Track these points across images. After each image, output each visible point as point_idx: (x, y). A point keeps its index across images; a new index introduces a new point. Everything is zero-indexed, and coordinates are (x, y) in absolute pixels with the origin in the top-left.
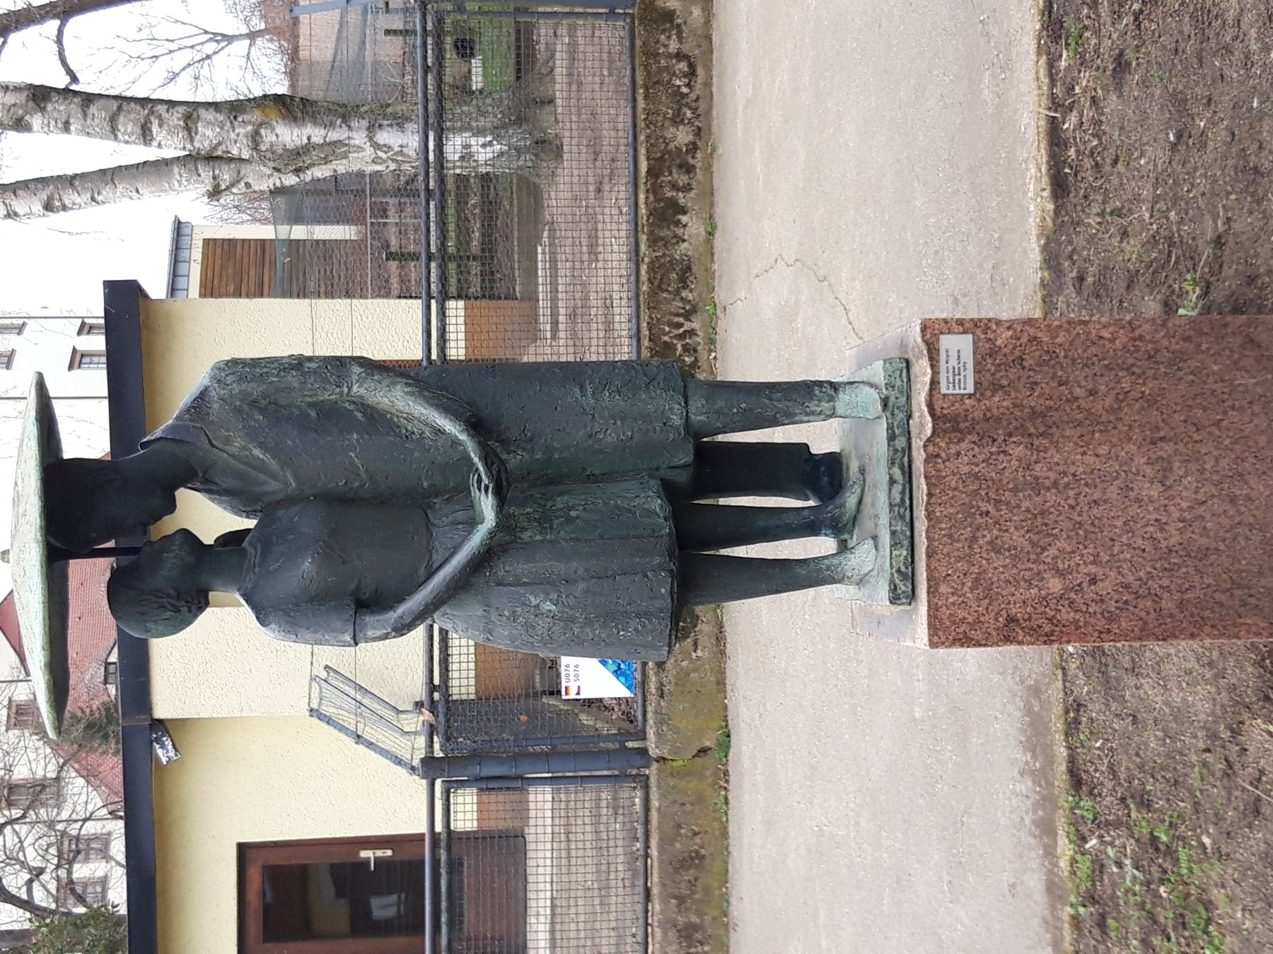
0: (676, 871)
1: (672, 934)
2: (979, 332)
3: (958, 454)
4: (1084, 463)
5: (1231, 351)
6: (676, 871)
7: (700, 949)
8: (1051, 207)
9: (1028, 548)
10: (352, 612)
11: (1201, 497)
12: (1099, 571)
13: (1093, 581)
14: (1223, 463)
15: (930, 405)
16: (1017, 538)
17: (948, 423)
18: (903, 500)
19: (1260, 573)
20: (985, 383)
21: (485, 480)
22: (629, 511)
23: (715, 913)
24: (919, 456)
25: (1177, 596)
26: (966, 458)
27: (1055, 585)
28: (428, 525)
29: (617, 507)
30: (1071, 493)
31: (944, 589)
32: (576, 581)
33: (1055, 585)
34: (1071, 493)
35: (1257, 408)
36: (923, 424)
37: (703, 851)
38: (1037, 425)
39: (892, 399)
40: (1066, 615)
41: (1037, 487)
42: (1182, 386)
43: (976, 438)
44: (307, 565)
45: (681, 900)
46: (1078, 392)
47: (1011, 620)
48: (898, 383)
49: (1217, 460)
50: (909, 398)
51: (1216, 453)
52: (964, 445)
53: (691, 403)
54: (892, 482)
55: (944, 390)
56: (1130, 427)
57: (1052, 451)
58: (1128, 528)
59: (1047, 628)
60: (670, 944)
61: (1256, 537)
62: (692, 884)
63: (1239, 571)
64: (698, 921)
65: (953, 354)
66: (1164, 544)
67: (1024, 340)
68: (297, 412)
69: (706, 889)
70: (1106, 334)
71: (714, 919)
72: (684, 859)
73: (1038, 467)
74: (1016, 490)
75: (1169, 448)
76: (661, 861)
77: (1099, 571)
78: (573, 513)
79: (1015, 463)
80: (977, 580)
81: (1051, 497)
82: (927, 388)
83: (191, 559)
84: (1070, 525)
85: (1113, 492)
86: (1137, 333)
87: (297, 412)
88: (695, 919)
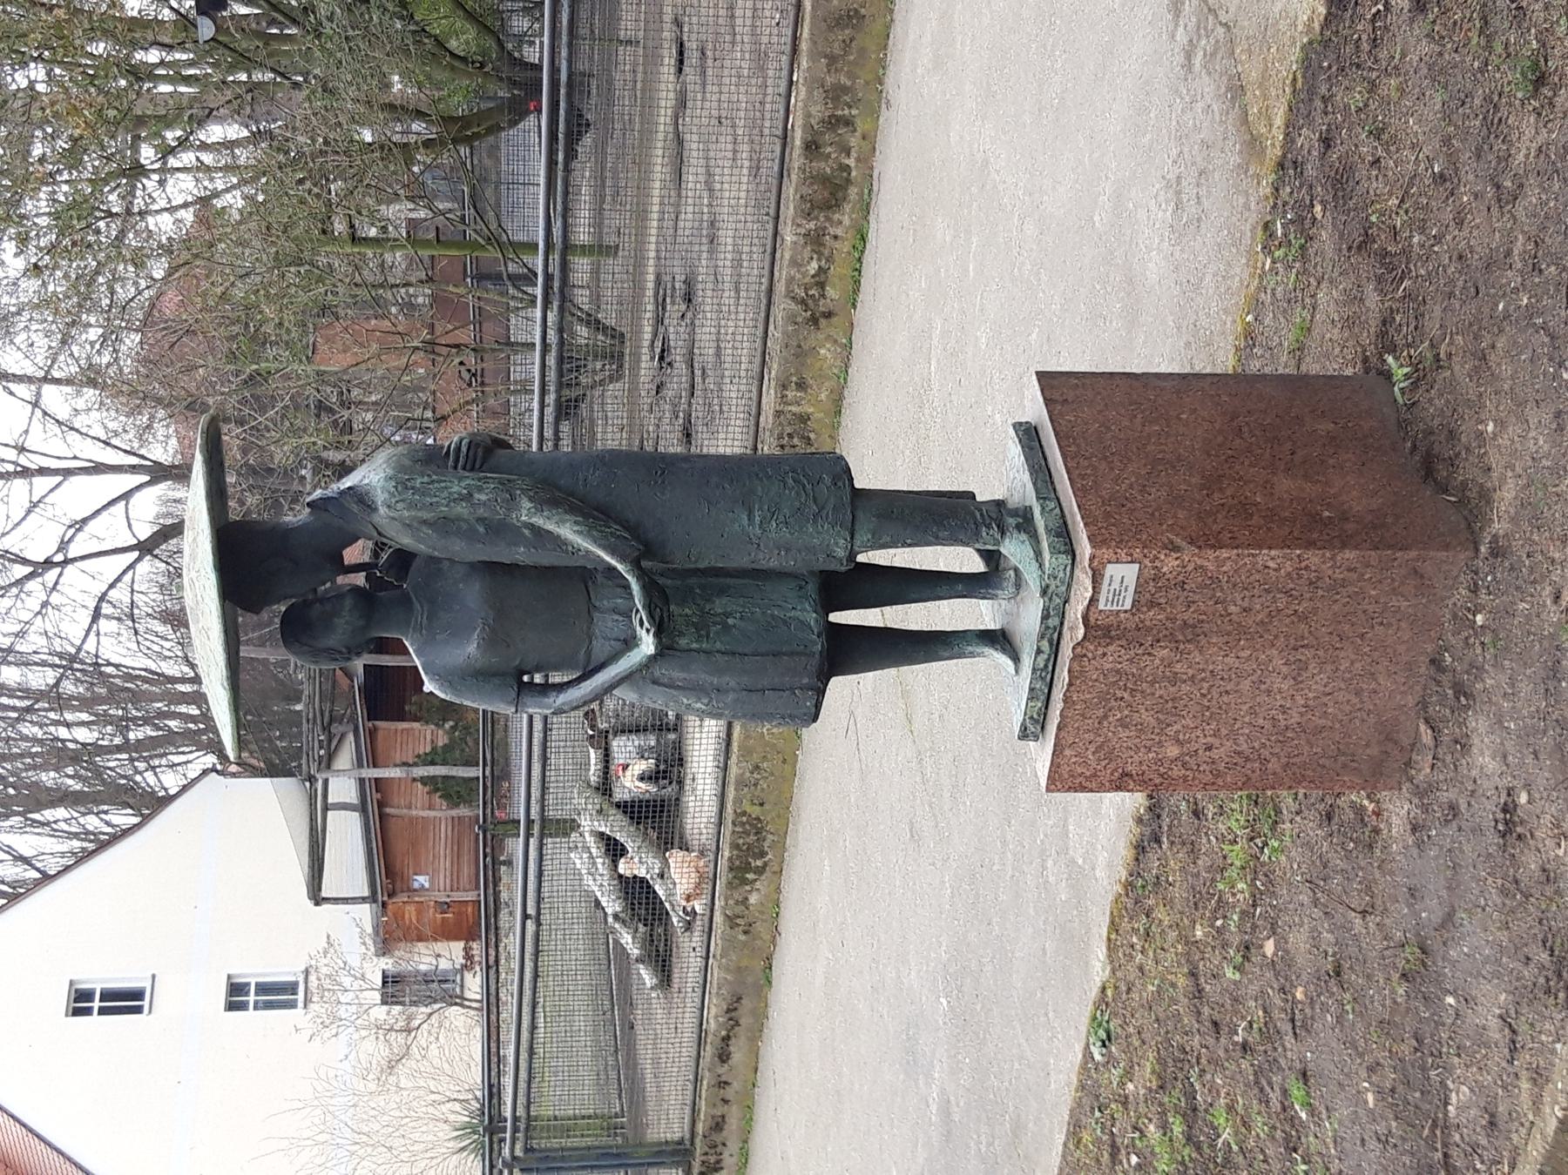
0: (830, 29)
1: (818, 94)
2: (1147, 561)
3: (1104, 654)
4: (1223, 662)
5: (1393, 580)
6: (830, 29)
7: (846, 112)
8: (1323, 10)
9: (1153, 722)
10: (514, 695)
11: (1327, 690)
12: (1216, 742)
13: (1209, 748)
14: (1358, 665)
15: (1085, 618)
16: (1147, 717)
17: (1099, 630)
18: (1046, 666)
19: (1367, 745)
20: (1143, 601)
21: (646, 624)
22: (785, 622)
23: (870, 77)
24: (1066, 652)
25: (1284, 760)
26: (1113, 656)
27: (1173, 751)
28: (591, 608)
29: (772, 616)
30: (1206, 685)
31: (1067, 752)
32: (727, 691)
33: (1173, 751)
34: (1206, 685)
35: (1403, 624)
36: (1075, 631)
37: (863, 11)
38: (1188, 634)
39: (1053, 587)
40: (1177, 772)
41: (1174, 680)
42: (1336, 607)
43: (1124, 642)
44: (472, 648)
45: (832, 59)
46: (1232, 609)
47: (1125, 774)
48: (1061, 575)
49: (1352, 663)
50: (1069, 586)
51: (1353, 657)
52: (1111, 648)
53: (857, 536)
54: (1039, 651)
55: (1101, 607)
56: (1276, 637)
57: (1196, 653)
58: (1253, 712)
59: (1157, 781)
60: (815, 103)
61: (1372, 719)
62: (847, 44)
63: (1348, 744)
64: (849, 83)
65: (1117, 580)
66: (1283, 723)
67: (1190, 567)
68: (465, 526)
69: (862, 51)
70: (1272, 564)
71: (867, 83)
72: (841, 17)
73: (1179, 666)
74: (1152, 683)
75: (1309, 653)
76: (813, 17)
77: (1216, 742)
78: (730, 621)
79: (1157, 662)
80: (1100, 747)
81: (1185, 688)
82: (1086, 603)
83: (361, 623)
84: (1198, 708)
85: (1246, 685)
86: (1303, 564)
87: (465, 526)
88: (844, 80)
